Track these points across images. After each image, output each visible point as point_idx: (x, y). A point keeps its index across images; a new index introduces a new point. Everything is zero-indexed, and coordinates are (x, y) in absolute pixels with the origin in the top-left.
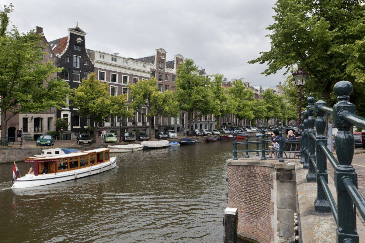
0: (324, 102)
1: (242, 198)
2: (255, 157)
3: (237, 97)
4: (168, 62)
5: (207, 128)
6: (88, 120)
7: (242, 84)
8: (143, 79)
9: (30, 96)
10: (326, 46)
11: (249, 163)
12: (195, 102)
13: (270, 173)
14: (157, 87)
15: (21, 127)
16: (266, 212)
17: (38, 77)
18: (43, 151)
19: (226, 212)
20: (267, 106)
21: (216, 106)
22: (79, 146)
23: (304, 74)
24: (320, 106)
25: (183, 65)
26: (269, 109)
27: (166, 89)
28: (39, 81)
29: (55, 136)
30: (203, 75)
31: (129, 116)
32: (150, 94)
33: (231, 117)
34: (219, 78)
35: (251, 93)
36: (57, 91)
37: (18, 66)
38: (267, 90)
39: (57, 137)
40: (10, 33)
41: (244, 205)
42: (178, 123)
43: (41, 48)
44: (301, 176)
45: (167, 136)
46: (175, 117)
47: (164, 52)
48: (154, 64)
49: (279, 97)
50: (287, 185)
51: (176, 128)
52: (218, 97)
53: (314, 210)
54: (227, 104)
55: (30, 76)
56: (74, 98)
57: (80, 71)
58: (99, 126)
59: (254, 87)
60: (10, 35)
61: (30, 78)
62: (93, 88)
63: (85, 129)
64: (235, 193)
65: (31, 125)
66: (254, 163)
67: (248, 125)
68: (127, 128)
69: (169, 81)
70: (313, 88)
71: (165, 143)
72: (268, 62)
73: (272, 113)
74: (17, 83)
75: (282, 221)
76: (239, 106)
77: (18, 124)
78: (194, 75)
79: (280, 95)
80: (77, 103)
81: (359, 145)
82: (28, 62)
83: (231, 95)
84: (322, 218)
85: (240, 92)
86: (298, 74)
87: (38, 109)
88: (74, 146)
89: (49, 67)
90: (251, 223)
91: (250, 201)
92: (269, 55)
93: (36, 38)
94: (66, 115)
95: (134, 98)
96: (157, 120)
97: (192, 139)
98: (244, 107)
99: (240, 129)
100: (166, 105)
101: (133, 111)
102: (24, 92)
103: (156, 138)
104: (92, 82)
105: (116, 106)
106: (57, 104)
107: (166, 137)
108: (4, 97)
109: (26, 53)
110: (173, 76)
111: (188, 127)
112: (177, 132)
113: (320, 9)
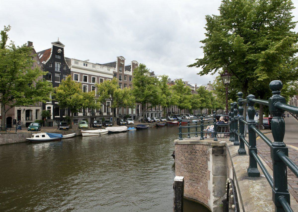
0: (254, 96)
1: (186, 169)
2: (195, 138)
3: (179, 92)
4: (126, 67)
5: (156, 116)
6: (66, 111)
7: (182, 83)
8: (107, 79)
9: (23, 93)
10: (243, 55)
11: (191, 142)
12: (147, 96)
13: (207, 150)
14: (118, 85)
15: (16, 117)
16: (204, 178)
17: (29, 79)
18: (33, 135)
19: (176, 179)
20: (201, 99)
21: (163, 99)
22: (60, 131)
23: (229, 75)
24: (250, 99)
25: (137, 68)
26: (203, 101)
27: (125, 87)
28: (29, 82)
29: (42, 123)
30: (153, 76)
31: (97, 108)
32: (113, 91)
33: (175, 108)
34: (165, 78)
35: (189, 89)
36: (43, 90)
37: (14, 71)
38: (201, 87)
39: (43, 124)
40: (9, 46)
41: (187, 174)
42: (134, 112)
43: (31, 57)
44: (234, 151)
45: (126, 122)
46: (132, 108)
47: (123, 59)
48: (116, 68)
49: (209, 92)
50: (220, 158)
51: (133, 116)
52: (165, 92)
53: (247, 175)
54: (171, 97)
55: (23, 78)
56: (56, 94)
57: (60, 74)
58: (74, 115)
59: (191, 85)
60: (9, 48)
61: (23, 80)
62: (69, 87)
63: (63, 118)
64: (181, 165)
65: (23, 115)
66: (195, 142)
67: (187, 114)
68: (96, 117)
69: (127, 81)
70: (235, 86)
71: (124, 128)
72: (202, 66)
73: (204, 105)
74: (14, 83)
75: (216, 184)
76: (180, 99)
77: (14, 115)
78: (147, 76)
79: (210, 91)
80: (58, 98)
81: (267, 127)
82: (22, 67)
83: (174, 91)
84: (254, 181)
85: (181, 89)
86: (225, 75)
87: (29, 103)
88: (56, 131)
89: (38, 71)
90: (193, 187)
91: (192, 171)
92: (202, 61)
93: (28, 50)
94: (49, 108)
95: (101, 94)
96: (118, 111)
97: (145, 124)
98: (184, 100)
99: (182, 117)
100: (125, 99)
101: (99, 103)
102: (19, 90)
103: (117, 124)
104: (69, 82)
105: (87, 100)
106: (43, 99)
107: (125, 124)
108: (4, 95)
109: (20, 61)
110: (130, 77)
111: (142, 115)
112: (134, 119)
113: (237, 29)
